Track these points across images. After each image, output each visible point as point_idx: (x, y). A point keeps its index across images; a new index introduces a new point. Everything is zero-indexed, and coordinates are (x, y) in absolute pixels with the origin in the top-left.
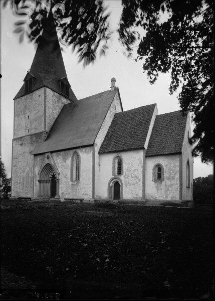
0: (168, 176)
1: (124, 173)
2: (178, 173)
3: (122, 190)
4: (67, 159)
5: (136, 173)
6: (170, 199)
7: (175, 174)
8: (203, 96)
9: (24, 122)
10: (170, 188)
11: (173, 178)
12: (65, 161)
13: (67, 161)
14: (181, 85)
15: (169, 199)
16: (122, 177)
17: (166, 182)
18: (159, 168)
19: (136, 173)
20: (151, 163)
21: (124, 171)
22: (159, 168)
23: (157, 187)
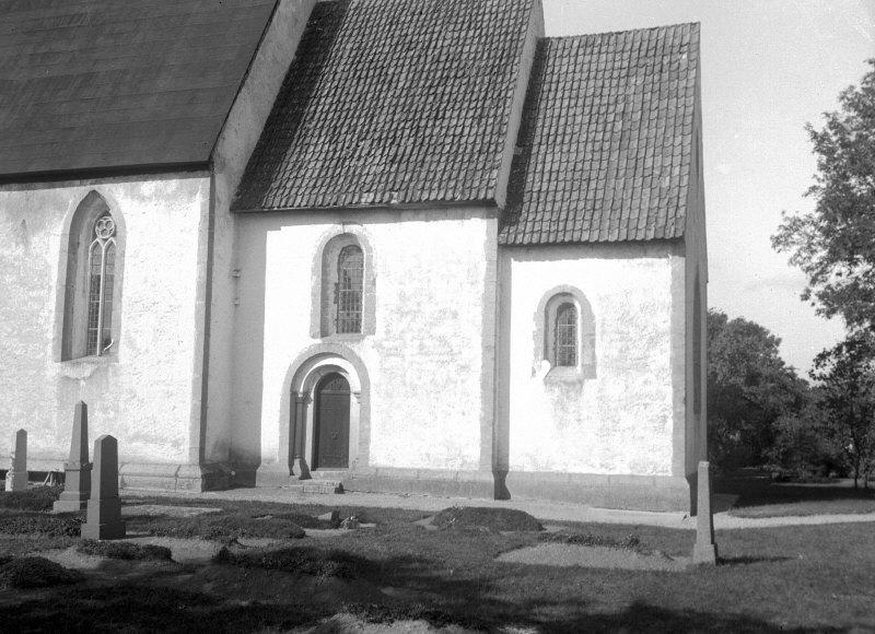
0: (615, 353)
1: (380, 326)
2: (668, 338)
3: (365, 417)
4: (39, 227)
5: (445, 329)
6: (627, 472)
7: (653, 342)
8: (828, 161)
9: (711, 423)
10: (627, 419)
11: (641, 365)
12: (25, 242)
13: (35, 240)
14: (811, 380)
15: (621, 468)
16: (366, 349)
17: (605, 387)
18: (562, 311)
19: (445, 329)
20: (535, 279)
21: (381, 315)
22: (562, 311)
23: (560, 405)
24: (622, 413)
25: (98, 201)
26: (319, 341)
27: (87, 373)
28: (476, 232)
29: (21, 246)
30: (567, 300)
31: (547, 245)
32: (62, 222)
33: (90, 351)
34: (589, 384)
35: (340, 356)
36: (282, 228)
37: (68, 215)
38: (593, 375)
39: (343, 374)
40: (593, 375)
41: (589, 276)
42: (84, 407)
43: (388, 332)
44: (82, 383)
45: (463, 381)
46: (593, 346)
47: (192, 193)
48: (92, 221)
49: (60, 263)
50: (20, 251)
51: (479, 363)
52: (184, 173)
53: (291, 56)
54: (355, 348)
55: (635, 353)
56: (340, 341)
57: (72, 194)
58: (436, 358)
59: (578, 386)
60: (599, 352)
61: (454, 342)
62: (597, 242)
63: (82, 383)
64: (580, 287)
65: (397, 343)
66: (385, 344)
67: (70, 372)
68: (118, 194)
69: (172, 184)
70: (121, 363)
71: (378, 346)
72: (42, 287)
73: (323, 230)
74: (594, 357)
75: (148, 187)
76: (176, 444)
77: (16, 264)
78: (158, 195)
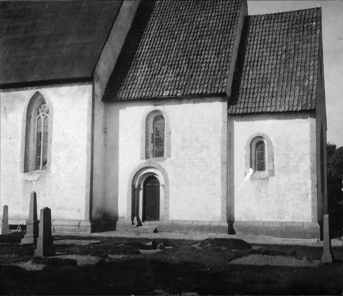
20: (245, 130)
22: (258, 144)
25: (40, 97)
27: (36, 178)
28: (217, 109)
30: (260, 139)
34: (271, 179)
35: (155, 168)
39: (156, 176)
42: (35, 194)
44: (34, 183)
46: (273, 161)
47: (84, 92)
48: (36, 105)
54: (162, 164)
56: (155, 161)
59: (267, 180)
63: (34, 183)
67: (28, 177)
68: (48, 93)
69: (75, 88)
74: (273, 166)
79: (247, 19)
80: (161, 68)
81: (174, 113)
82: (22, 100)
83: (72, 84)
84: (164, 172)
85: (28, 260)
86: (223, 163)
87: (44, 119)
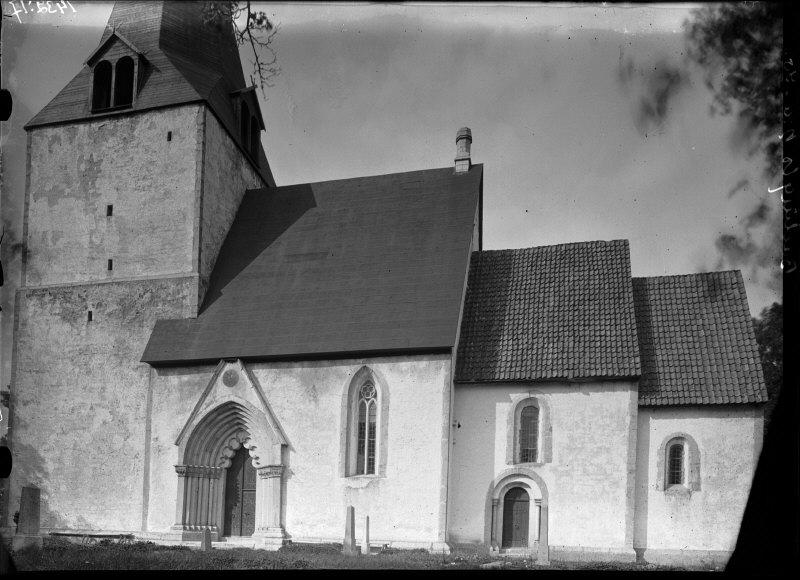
12: (315, 398)
16: (546, 472)
20: (662, 429)
22: (675, 452)
24: (718, 513)
25: (365, 374)
26: (512, 467)
27: (364, 484)
28: (623, 399)
29: (313, 403)
30: (679, 442)
31: (676, 406)
32: (537, 396)
33: (360, 471)
34: (695, 495)
35: (525, 476)
36: (591, 394)
37: (347, 382)
38: (698, 489)
39: (527, 489)
40: (698, 489)
41: (696, 428)
42: (353, 509)
43: (561, 461)
44: (360, 490)
45: (614, 492)
46: (699, 471)
47: (438, 369)
48: (363, 389)
49: (342, 414)
50: (312, 406)
51: (625, 481)
52: (432, 355)
53: (227, 228)
54: (537, 471)
55: (728, 475)
56: (526, 467)
57: (348, 370)
58: (594, 477)
59: (688, 496)
60: (703, 474)
61: (608, 468)
62: (728, 404)
63: (360, 490)
64: (688, 433)
65: (567, 468)
66: (560, 468)
67: (353, 483)
68: (382, 370)
69: (423, 364)
70: (388, 477)
71: (554, 470)
72: (329, 430)
73: (518, 396)
74: (699, 478)
75: (405, 365)
76: (429, 530)
77: (310, 414)
78: (414, 370)
79: (640, 285)
80: (362, 406)
81: (558, 405)
82: (340, 377)
83: (437, 356)
84: (541, 483)
85: (769, 395)
86: (630, 472)
87: (370, 406)
